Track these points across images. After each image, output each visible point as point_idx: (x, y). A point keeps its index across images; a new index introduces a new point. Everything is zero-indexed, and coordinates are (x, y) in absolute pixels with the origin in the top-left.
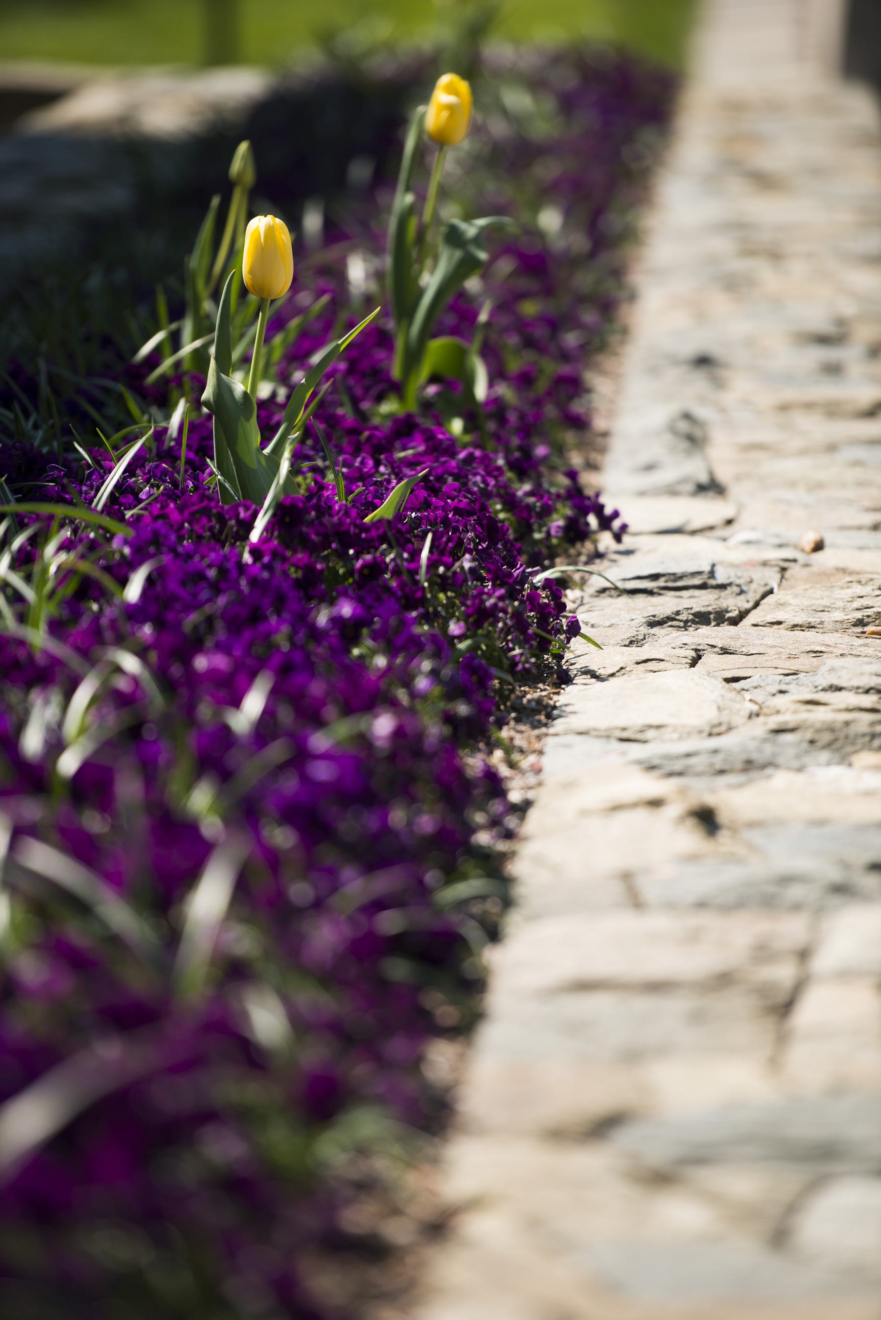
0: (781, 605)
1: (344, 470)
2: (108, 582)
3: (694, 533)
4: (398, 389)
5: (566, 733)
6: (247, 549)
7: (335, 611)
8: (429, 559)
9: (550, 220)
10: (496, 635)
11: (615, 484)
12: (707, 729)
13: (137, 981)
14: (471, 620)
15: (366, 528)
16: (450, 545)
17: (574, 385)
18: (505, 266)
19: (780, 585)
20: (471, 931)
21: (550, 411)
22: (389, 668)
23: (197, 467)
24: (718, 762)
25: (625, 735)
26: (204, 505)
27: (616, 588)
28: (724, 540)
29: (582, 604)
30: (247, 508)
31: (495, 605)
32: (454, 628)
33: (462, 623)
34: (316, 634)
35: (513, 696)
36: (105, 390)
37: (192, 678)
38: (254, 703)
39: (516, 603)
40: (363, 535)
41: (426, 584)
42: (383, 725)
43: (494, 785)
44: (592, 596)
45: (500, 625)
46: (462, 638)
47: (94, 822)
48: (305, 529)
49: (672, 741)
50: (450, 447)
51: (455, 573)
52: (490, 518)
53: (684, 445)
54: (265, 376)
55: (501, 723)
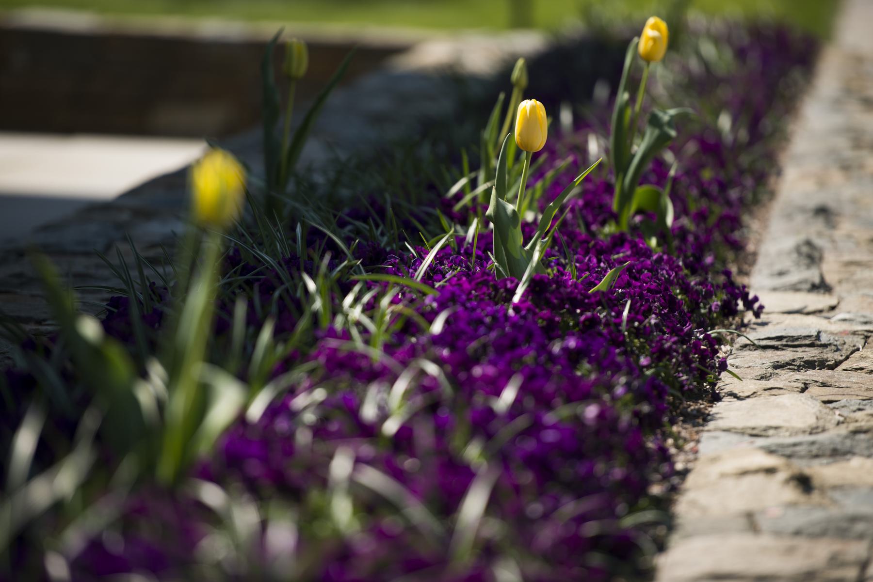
0: (863, 358)
1: (578, 265)
2: (421, 321)
3: (808, 314)
4: (615, 217)
5: (716, 429)
6: (511, 306)
7: (565, 343)
8: (628, 317)
9: (725, 122)
10: (671, 367)
11: (758, 283)
12: (809, 430)
13: (425, 549)
14: (655, 356)
15: (589, 297)
16: (643, 308)
17: (735, 222)
18: (691, 148)
19: (863, 347)
20: (645, 542)
21: (717, 236)
22: (597, 380)
23: (483, 260)
24: (814, 449)
25: (754, 432)
26: (486, 280)
27: (754, 345)
28: (829, 318)
29: (731, 354)
30: (512, 282)
31: (670, 347)
32: (643, 361)
33: (649, 358)
34: (553, 359)
35: (681, 407)
36: (427, 214)
37: (471, 380)
38: (509, 395)
39: (685, 347)
40: (586, 301)
41: (626, 333)
42: (591, 411)
43: (664, 456)
44: (737, 349)
45: (674, 360)
46: (648, 367)
47: (408, 464)
48: (548, 295)
49: (784, 437)
50: (648, 252)
51: (645, 326)
52: (671, 296)
53: (806, 261)
54: (530, 207)
55: (673, 422)
